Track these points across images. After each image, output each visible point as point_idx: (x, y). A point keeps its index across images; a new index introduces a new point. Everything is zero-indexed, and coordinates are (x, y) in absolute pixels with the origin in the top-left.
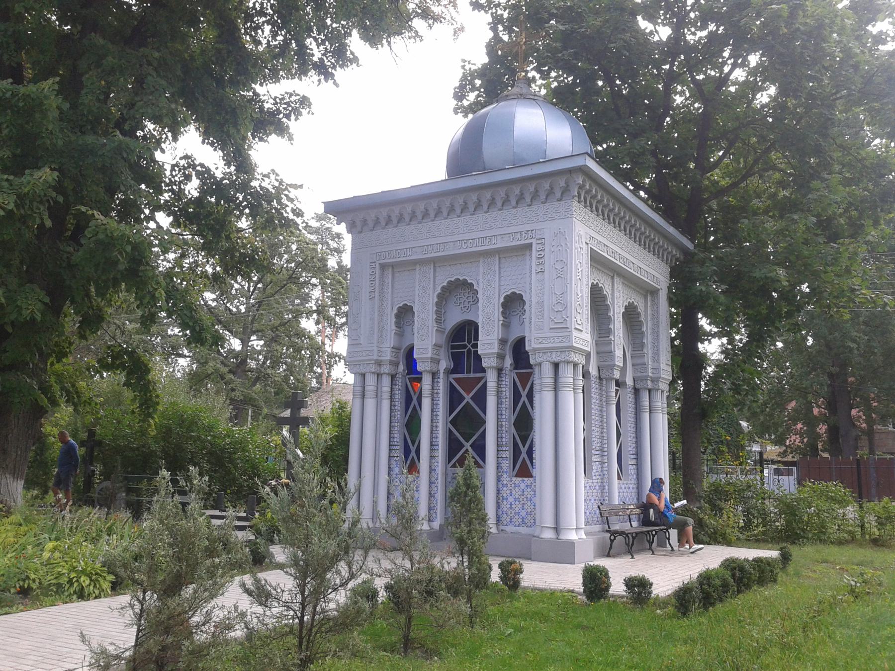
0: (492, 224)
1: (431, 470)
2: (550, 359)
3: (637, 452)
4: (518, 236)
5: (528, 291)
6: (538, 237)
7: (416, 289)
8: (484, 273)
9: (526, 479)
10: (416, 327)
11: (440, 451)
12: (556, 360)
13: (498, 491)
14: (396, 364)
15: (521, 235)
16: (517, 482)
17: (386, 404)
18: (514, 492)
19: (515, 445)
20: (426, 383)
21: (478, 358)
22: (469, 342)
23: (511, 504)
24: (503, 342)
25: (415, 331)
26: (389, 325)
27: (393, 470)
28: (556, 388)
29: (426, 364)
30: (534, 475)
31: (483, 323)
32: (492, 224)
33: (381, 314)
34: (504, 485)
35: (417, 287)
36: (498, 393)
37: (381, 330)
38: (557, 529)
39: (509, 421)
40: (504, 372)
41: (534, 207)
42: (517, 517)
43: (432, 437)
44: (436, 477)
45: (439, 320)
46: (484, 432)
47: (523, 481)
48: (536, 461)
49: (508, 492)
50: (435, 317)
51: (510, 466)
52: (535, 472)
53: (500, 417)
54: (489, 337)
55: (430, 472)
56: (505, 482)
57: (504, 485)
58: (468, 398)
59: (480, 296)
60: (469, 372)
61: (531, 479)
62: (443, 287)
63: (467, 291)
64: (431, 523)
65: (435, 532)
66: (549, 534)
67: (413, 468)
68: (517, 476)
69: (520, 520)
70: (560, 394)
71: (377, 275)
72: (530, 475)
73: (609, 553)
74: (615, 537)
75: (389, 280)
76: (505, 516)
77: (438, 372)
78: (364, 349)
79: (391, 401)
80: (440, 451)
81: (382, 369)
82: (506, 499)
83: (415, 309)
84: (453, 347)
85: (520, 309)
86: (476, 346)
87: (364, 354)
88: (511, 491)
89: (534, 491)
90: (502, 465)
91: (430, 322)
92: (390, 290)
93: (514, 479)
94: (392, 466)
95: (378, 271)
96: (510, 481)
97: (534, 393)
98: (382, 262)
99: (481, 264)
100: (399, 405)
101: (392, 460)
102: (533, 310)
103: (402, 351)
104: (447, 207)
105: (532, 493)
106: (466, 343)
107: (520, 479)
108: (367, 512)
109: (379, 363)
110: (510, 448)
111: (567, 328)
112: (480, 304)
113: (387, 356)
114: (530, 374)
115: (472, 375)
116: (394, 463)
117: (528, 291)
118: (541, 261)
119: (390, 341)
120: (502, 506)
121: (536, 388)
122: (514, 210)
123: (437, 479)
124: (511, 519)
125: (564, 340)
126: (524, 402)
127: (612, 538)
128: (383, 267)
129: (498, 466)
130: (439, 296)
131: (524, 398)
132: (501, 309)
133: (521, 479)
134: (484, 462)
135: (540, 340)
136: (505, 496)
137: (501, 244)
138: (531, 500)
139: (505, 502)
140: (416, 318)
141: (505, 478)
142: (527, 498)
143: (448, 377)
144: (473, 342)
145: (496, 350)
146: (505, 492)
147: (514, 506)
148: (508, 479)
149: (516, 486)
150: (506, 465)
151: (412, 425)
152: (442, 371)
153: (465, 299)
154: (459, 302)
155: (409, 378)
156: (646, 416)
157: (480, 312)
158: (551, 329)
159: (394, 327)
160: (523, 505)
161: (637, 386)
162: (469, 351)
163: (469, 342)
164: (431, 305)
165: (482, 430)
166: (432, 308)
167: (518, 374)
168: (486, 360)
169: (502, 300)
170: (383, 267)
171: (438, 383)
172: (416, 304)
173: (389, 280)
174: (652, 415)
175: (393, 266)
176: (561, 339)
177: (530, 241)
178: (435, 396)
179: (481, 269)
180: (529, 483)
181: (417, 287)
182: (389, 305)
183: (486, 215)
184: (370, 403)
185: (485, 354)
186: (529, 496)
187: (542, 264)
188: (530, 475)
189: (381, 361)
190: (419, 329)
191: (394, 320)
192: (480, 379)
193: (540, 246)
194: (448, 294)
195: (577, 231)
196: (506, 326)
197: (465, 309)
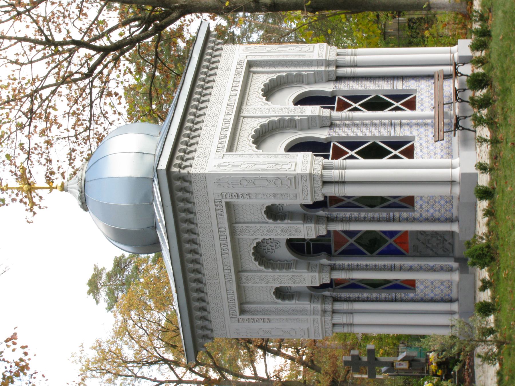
0: (209, 230)
1: (411, 269)
2: (320, 189)
4: (219, 212)
6: (220, 197)
7: (261, 285)
8: (248, 235)
12: (320, 183)
14: (324, 298)
15: (219, 210)
16: (418, 207)
17: (358, 306)
18: (427, 289)
19: (389, 206)
23: (436, 211)
26: (291, 306)
28: (343, 183)
29: (324, 276)
32: (209, 230)
33: (283, 312)
35: (259, 285)
36: (353, 269)
37: (296, 312)
38: (452, 182)
39: (371, 212)
40: (329, 216)
41: (195, 200)
42: (445, 206)
45: (286, 265)
47: (417, 202)
49: (426, 213)
50: (284, 271)
53: (367, 219)
54: (302, 230)
58: (351, 241)
62: (259, 264)
64: (453, 269)
65: (460, 265)
66: (457, 190)
67: (410, 285)
69: (448, 204)
70: (346, 180)
71: (249, 317)
73: (473, 131)
74: (460, 126)
75: (253, 307)
77: (330, 265)
78: (312, 325)
81: (328, 310)
82: (432, 214)
83: (278, 286)
84: (309, 253)
87: (317, 325)
88: (425, 211)
90: (405, 217)
91: (289, 274)
92: (262, 306)
93: (416, 209)
95: (245, 317)
98: (238, 313)
99: (241, 237)
100: (358, 294)
101: (404, 299)
103: (312, 293)
104: (194, 265)
107: (416, 205)
108: (445, 320)
109: (324, 312)
110: (391, 211)
111: (295, 177)
113: (318, 306)
119: (305, 305)
122: (197, 214)
123: (418, 265)
124: (447, 211)
125: (305, 179)
127: (460, 128)
128: (242, 312)
130: (267, 267)
132: (279, 221)
135: (305, 196)
137: (225, 224)
141: (415, 215)
143: (334, 256)
145: (312, 226)
146: (427, 215)
147: (437, 209)
148: (416, 213)
150: (405, 214)
151: (375, 285)
154: (271, 250)
155: (336, 286)
157: (281, 237)
158: (295, 188)
159: (293, 302)
161: (334, 78)
164: (274, 274)
168: (320, 232)
169: (271, 221)
171: (339, 265)
172: (273, 285)
173: (253, 307)
174: (358, 65)
175: (241, 303)
176: (304, 181)
179: (245, 236)
180: (419, 283)
181: (259, 285)
182: (275, 306)
183: (201, 235)
185: (316, 233)
187: (242, 195)
189: (322, 311)
191: (287, 302)
193: (228, 196)
194: (264, 258)
195: (215, 169)
197: (278, 245)
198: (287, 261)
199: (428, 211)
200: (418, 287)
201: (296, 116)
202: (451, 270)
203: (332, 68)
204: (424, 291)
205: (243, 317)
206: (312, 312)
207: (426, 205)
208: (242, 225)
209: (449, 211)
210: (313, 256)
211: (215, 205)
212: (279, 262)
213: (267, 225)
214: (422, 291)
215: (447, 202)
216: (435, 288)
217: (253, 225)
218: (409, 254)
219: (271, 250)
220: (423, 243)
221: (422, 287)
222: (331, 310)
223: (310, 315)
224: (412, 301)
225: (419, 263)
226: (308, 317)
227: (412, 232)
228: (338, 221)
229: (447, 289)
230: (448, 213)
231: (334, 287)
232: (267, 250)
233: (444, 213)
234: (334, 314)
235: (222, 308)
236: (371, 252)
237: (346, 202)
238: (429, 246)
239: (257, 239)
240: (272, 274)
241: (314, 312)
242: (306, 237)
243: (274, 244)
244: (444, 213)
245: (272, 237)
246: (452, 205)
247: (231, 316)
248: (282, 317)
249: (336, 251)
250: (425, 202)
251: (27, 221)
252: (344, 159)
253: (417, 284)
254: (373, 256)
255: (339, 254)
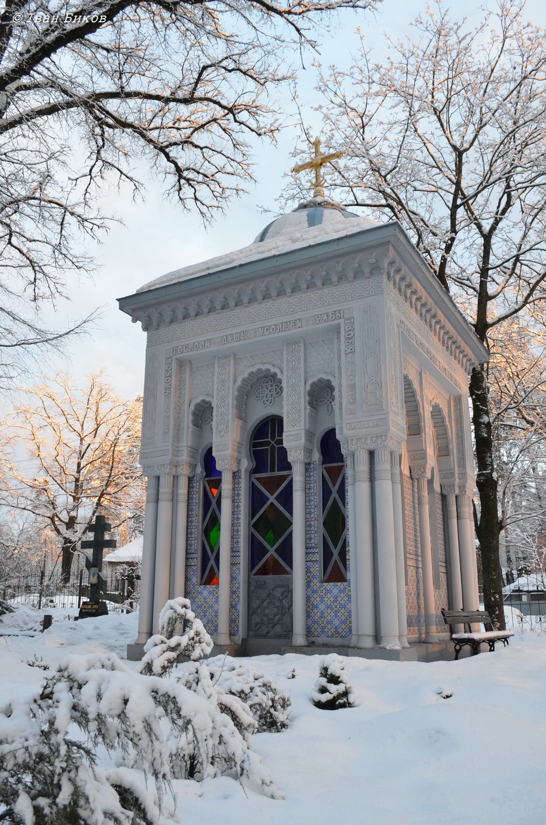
1: (233, 579)
3: (446, 559)
5: (337, 375)
6: (346, 316)
9: (339, 584)
10: (214, 424)
11: (242, 557)
13: (308, 599)
16: (328, 587)
20: (226, 486)
21: (283, 452)
22: (273, 438)
23: (336, 616)
24: (310, 435)
25: (214, 426)
26: (186, 422)
27: (190, 580)
28: (372, 479)
30: (348, 578)
31: (288, 413)
34: (314, 592)
35: (216, 381)
36: (307, 490)
40: (312, 466)
43: (233, 519)
44: (238, 585)
46: (291, 533)
48: (351, 563)
51: (320, 569)
52: (350, 575)
54: (295, 428)
55: (231, 581)
56: (315, 588)
57: (314, 592)
58: (272, 499)
59: (284, 385)
60: (273, 470)
61: (345, 584)
63: (270, 383)
68: (328, 581)
70: (377, 483)
71: (173, 370)
72: (343, 579)
74: (461, 647)
75: (187, 376)
76: (316, 626)
77: (239, 471)
79: (188, 506)
80: (242, 557)
81: (179, 470)
83: (214, 405)
84: (255, 445)
85: (328, 398)
86: (281, 442)
88: (322, 598)
89: (349, 597)
93: (325, 584)
94: (189, 576)
96: (320, 587)
97: (346, 488)
98: (178, 356)
100: (198, 510)
101: (189, 570)
102: (344, 394)
103: (200, 451)
105: (346, 599)
106: (269, 439)
107: (332, 584)
112: (284, 394)
114: (341, 468)
115: (277, 473)
116: (192, 573)
117: (337, 375)
118: (350, 341)
120: (312, 614)
121: (349, 481)
123: (239, 588)
126: (335, 498)
127: (458, 647)
129: (308, 571)
131: (335, 494)
132: (308, 398)
133: (333, 584)
134: (291, 568)
136: (315, 603)
138: (344, 606)
139: (315, 611)
140: (214, 414)
141: (316, 584)
142: (332, 609)
144: (277, 438)
148: (318, 584)
149: (328, 591)
150: (317, 569)
152: (243, 471)
153: (268, 391)
154: (261, 395)
155: (207, 481)
156: (454, 521)
159: (191, 425)
160: (336, 612)
161: (445, 493)
162: (273, 447)
163: (273, 438)
165: (288, 532)
166: (231, 402)
167: (326, 468)
169: (308, 387)
170: (181, 364)
177: (337, 322)
178: (235, 533)
179: (285, 357)
180: (211, 589)
184: (165, 507)
186: (343, 602)
187: (353, 344)
188: (343, 579)
190: (217, 424)
192: (286, 477)
196: (314, 418)
197: (268, 403)
198: (246, 416)
199: (322, 601)
200: (205, 588)
201: (425, 435)
202: (231, 634)
203: (457, 492)
204: (200, 597)
205: (174, 363)
206: (176, 449)
207: (332, 599)
208: (302, 354)
209: (323, 632)
210: (250, 450)
211: (335, 312)
212: (244, 406)
213: (302, 383)
214: (201, 593)
215: (336, 628)
216: (203, 611)
217: (302, 365)
218: (253, 577)
219: (261, 395)
220: (269, 594)
221: (205, 593)
222: (178, 474)
223: (172, 445)
224: (187, 579)
225: (241, 590)
226: (170, 443)
227: (291, 581)
228: (306, 476)
229: (333, 630)
230: (319, 630)
231: (207, 479)
232: (261, 390)
233: (319, 625)
234: (172, 477)
235: (187, 336)
236: (255, 526)
237: (332, 489)
238: (265, 604)
239: (282, 373)
240: (231, 395)
241: (176, 452)
242: (284, 434)
243: (270, 398)
244: (319, 625)
245: (285, 390)
246: (332, 636)
247: (175, 350)
248: (172, 411)
249: (257, 479)
250: (336, 597)
251: (30, 665)
252: (433, 468)
253: (210, 588)
254: (249, 528)
255: (253, 484)
